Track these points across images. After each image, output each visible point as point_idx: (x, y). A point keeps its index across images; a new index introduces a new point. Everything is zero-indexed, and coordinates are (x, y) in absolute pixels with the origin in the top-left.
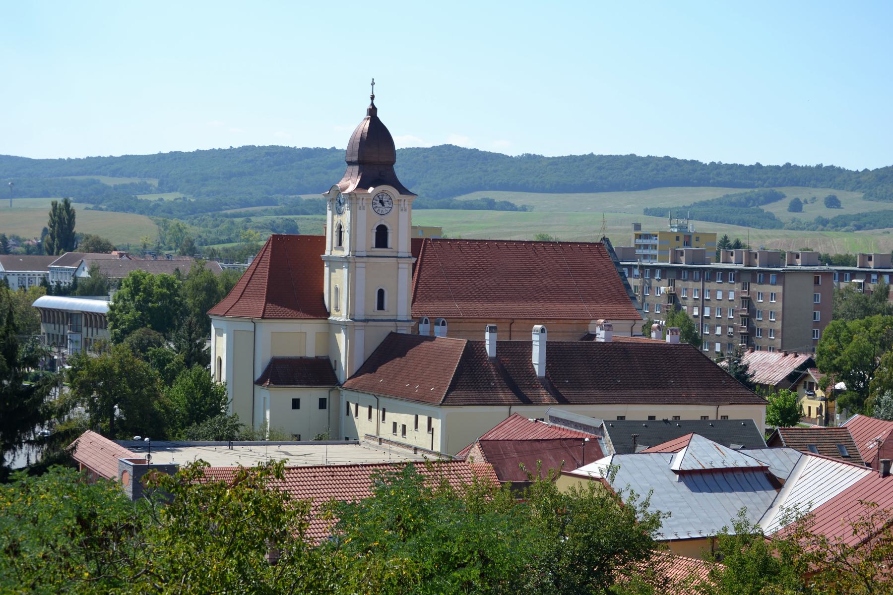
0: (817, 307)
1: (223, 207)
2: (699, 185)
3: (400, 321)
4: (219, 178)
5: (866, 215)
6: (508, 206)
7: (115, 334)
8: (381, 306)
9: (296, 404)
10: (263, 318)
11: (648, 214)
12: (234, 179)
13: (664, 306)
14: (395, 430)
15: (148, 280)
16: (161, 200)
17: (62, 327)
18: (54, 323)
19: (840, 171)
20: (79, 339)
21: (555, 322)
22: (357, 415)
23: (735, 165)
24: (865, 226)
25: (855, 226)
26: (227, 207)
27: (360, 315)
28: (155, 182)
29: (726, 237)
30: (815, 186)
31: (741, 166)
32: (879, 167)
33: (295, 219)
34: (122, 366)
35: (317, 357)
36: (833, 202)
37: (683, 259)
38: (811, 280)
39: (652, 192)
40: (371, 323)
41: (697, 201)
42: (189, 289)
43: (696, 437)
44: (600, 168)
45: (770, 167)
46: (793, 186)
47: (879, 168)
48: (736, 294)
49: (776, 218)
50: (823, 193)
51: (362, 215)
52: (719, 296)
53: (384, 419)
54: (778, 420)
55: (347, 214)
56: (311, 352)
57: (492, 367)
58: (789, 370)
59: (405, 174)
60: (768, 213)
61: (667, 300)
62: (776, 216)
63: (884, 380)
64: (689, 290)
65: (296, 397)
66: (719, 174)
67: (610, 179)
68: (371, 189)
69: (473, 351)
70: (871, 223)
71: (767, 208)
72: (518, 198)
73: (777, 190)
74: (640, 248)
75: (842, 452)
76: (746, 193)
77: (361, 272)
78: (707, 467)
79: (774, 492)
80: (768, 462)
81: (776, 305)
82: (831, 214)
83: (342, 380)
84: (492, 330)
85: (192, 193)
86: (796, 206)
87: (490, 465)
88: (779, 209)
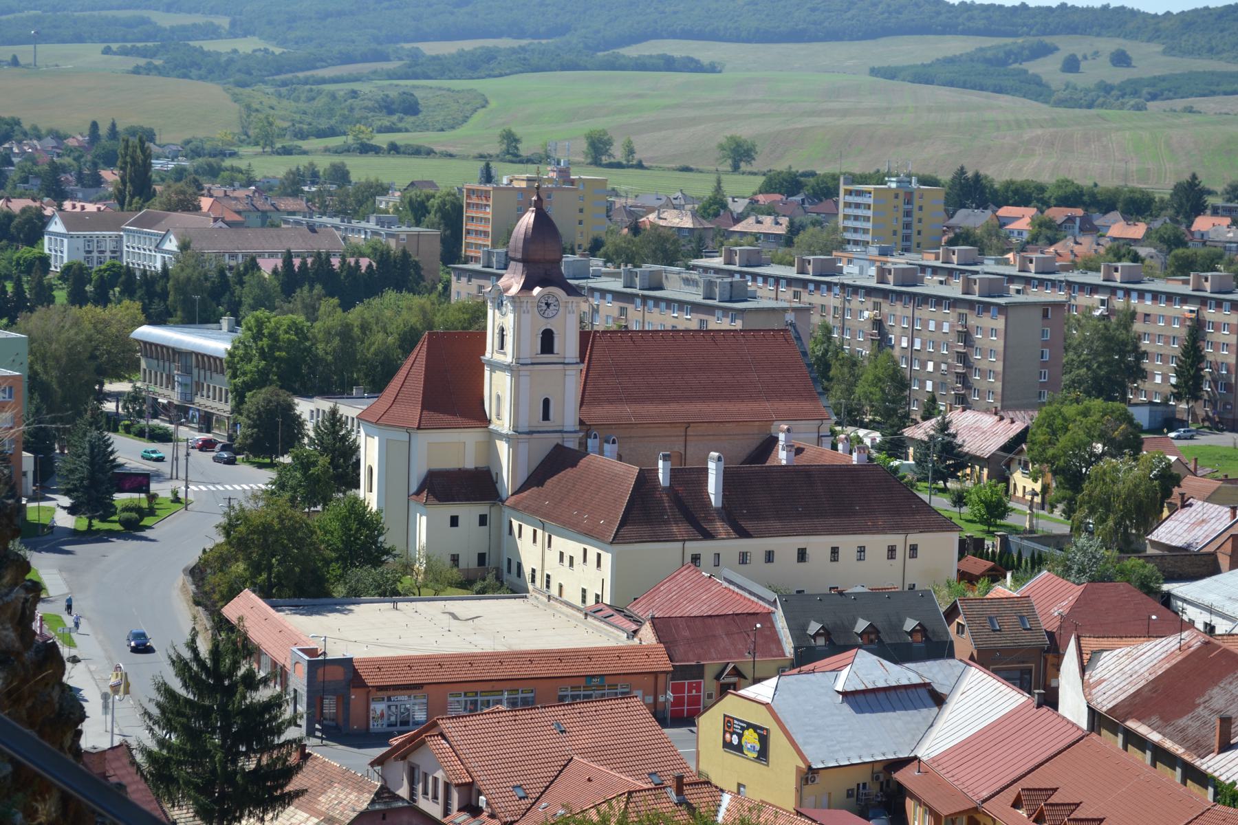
0: (1045, 344)
1: (318, 64)
2: (943, 32)
3: (566, 432)
4: (310, 18)
5: (1163, 79)
6: (692, 66)
7: (235, 385)
8: (546, 416)
9: (454, 521)
10: (419, 428)
11: (876, 76)
12: (330, 20)
13: (867, 334)
14: (561, 560)
15: (273, 324)
16: (235, 51)
17: (167, 364)
18: (157, 359)
19: (1134, 13)
20: (189, 382)
21: (735, 424)
22: (520, 536)
23: (993, 5)
24: (1162, 94)
25: (1149, 93)
26: (324, 64)
27: (524, 426)
28: (224, 22)
29: (962, 168)
30: (1099, 35)
31: (1001, 7)
32: (1186, 9)
33: (414, 87)
34: (281, 521)
35: (476, 468)
36: (1121, 59)
37: (891, 278)
38: (1038, 313)
39: (882, 41)
40: (535, 435)
41: (940, 55)
42: (319, 332)
43: (862, 652)
44: (813, 10)
45: (1039, 8)
46: (1069, 34)
47: (1186, 10)
48: (952, 326)
49: (1044, 81)
50: (1108, 45)
51: (527, 319)
52: (932, 326)
53: (549, 546)
54: (983, 516)
55: (510, 317)
56: (470, 462)
57: (665, 498)
58: (1002, 440)
59: (557, 15)
60: (1033, 75)
61: (871, 326)
62: (1045, 78)
63: (1094, 494)
64: (897, 315)
65: (455, 514)
66: (971, 18)
67: (826, 24)
68: (537, 290)
69: (645, 479)
70: (1170, 91)
71: (1035, 67)
72: (704, 52)
73: (1048, 40)
74: (850, 207)
75: (1024, 624)
76: (1006, 45)
77: (525, 381)
78: (870, 686)
79: (936, 709)
80: (930, 676)
81: (997, 342)
82: (1118, 76)
83: (504, 496)
84: (665, 458)
85: (275, 39)
86: (1072, 65)
87: (662, 645)
88: (1047, 69)
